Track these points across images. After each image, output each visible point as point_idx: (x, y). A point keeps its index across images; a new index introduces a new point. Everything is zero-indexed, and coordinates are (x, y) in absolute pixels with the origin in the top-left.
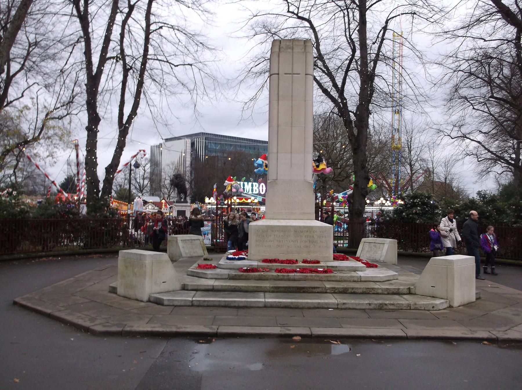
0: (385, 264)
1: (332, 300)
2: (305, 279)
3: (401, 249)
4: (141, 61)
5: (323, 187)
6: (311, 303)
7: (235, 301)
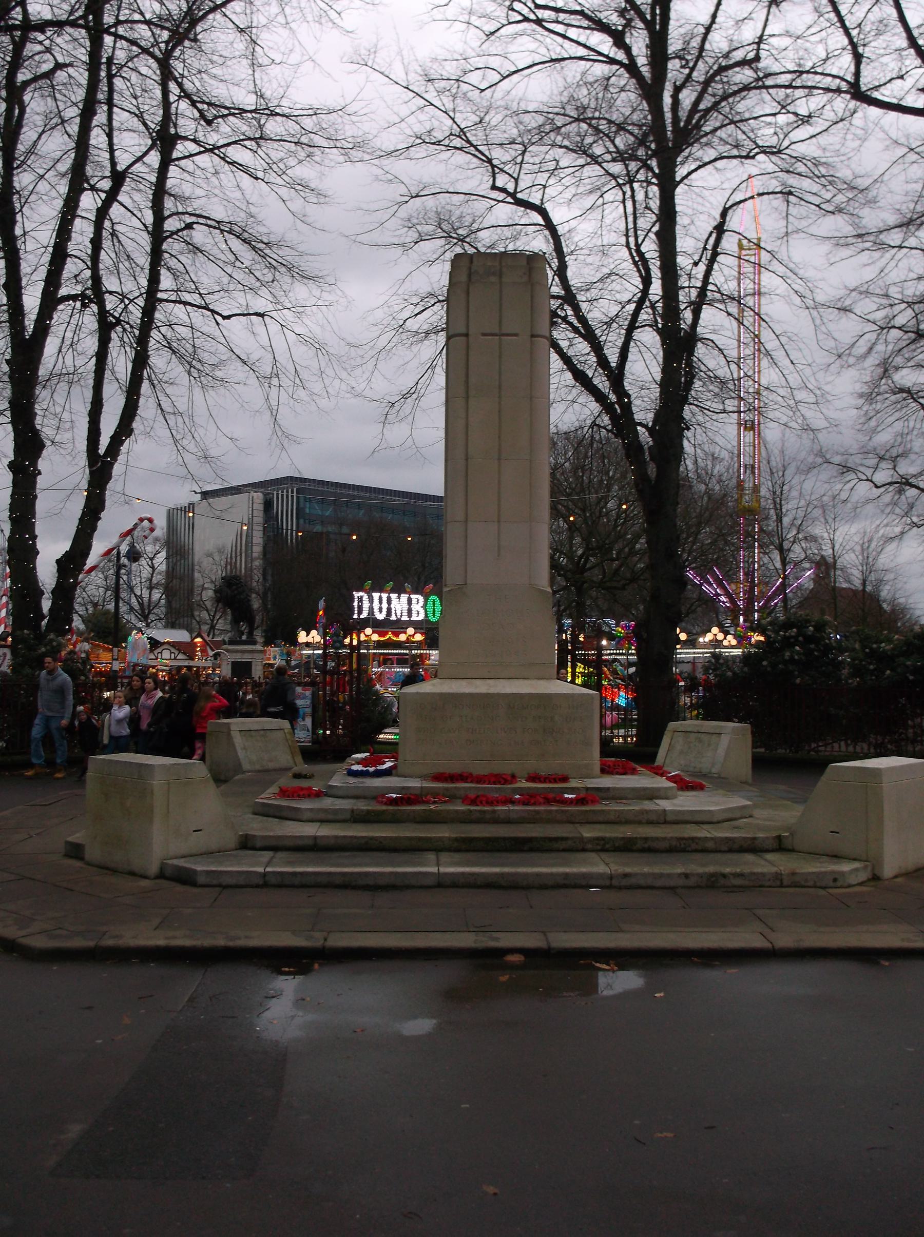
0: (723, 783)
1: (597, 866)
2: (534, 819)
3: (760, 747)
4: (142, 305)
5: (578, 603)
6: (547, 874)
7: (367, 874)
